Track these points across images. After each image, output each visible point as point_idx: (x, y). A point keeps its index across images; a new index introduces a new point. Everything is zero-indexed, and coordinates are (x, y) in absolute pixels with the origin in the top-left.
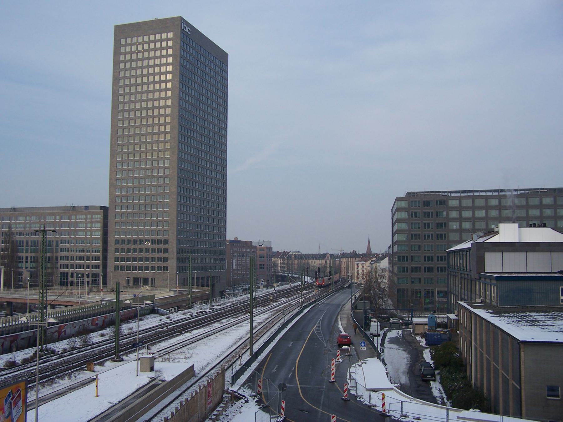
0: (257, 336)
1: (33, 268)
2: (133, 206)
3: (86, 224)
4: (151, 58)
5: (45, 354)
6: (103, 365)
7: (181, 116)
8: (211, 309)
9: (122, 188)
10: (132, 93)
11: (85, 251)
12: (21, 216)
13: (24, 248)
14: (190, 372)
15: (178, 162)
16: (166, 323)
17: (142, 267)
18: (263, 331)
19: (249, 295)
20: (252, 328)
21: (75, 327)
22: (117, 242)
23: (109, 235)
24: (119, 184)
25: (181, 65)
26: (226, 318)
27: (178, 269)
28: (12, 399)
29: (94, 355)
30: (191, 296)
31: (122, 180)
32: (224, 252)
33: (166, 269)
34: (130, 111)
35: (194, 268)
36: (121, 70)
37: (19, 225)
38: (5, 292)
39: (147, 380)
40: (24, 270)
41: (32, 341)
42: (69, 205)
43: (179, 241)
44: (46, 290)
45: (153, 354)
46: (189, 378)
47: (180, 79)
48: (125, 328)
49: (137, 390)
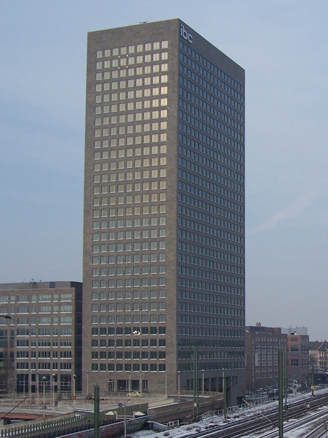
3: (52, 307)
7: (181, 157)
9: (100, 257)
22: (95, 331)
23: (83, 322)
24: (96, 252)
30: (198, 405)
31: (100, 245)
33: (163, 367)
42: (28, 281)
43: (180, 328)
47: (179, 105)
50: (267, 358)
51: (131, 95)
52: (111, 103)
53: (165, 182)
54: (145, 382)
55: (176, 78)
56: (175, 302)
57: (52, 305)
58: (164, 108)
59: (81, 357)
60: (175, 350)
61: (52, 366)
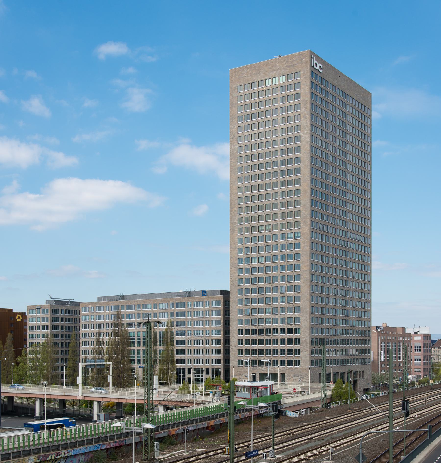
22: (240, 332)
23: (230, 324)
27: (313, 362)
33: (298, 362)
38: (114, 391)
43: (313, 330)
54: (283, 375)
61: (204, 361)
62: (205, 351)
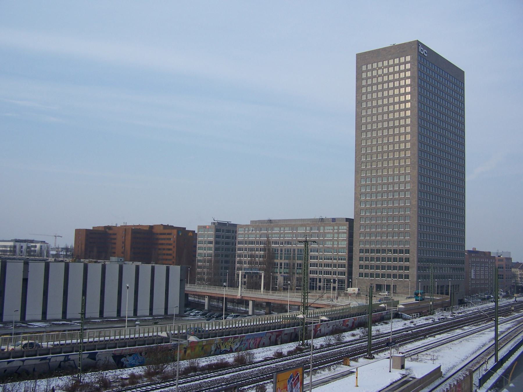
0: (500, 344)
1: (287, 273)
2: (377, 218)
3: (333, 234)
4: (391, 81)
5: (306, 349)
6: (357, 361)
7: (420, 134)
8: (452, 316)
9: (366, 202)
10: (374, 115)
11: (333, 259)
12: (276, 227)
13: (279, 255)
14: (437, 373)
15: (418, 177)
16: (410, 327)
17: (385, 275)
18: (508, 339)
19: (494, 303)
20: (496, 335)
21: (329, 327)
22: (361, 251)
24: (363, 198)
25: (419, 86)
26: (468, 326)
27: (419, 277)
28: (293, 381)
29: (348, 352)
30: (433, 303)
31: (366, 194)
32: (463, 262)
33: (407, 277)
34: (372, 130)
35: (436, 277)
36: (364, 94)
37: (275, 234)
39: (399, 377)
40: (278, 275)
41: (293, 336)
42: (318, 217)
43: (419, 250)
44: (308, 293)
45: (402, 353)
46: (436, 378)
47: (418, 99)
48: (374, 329)
49: (391, 384)
50: (480, 273)
51: (386, 94)
52: (372, 100)
53: (409, 152)
55: (416, 80)
56: (416, 233)
57: (333, 233)
58: (408, 101)
59: (352, 268)
60: (416, 266)
62: (333, 265)
